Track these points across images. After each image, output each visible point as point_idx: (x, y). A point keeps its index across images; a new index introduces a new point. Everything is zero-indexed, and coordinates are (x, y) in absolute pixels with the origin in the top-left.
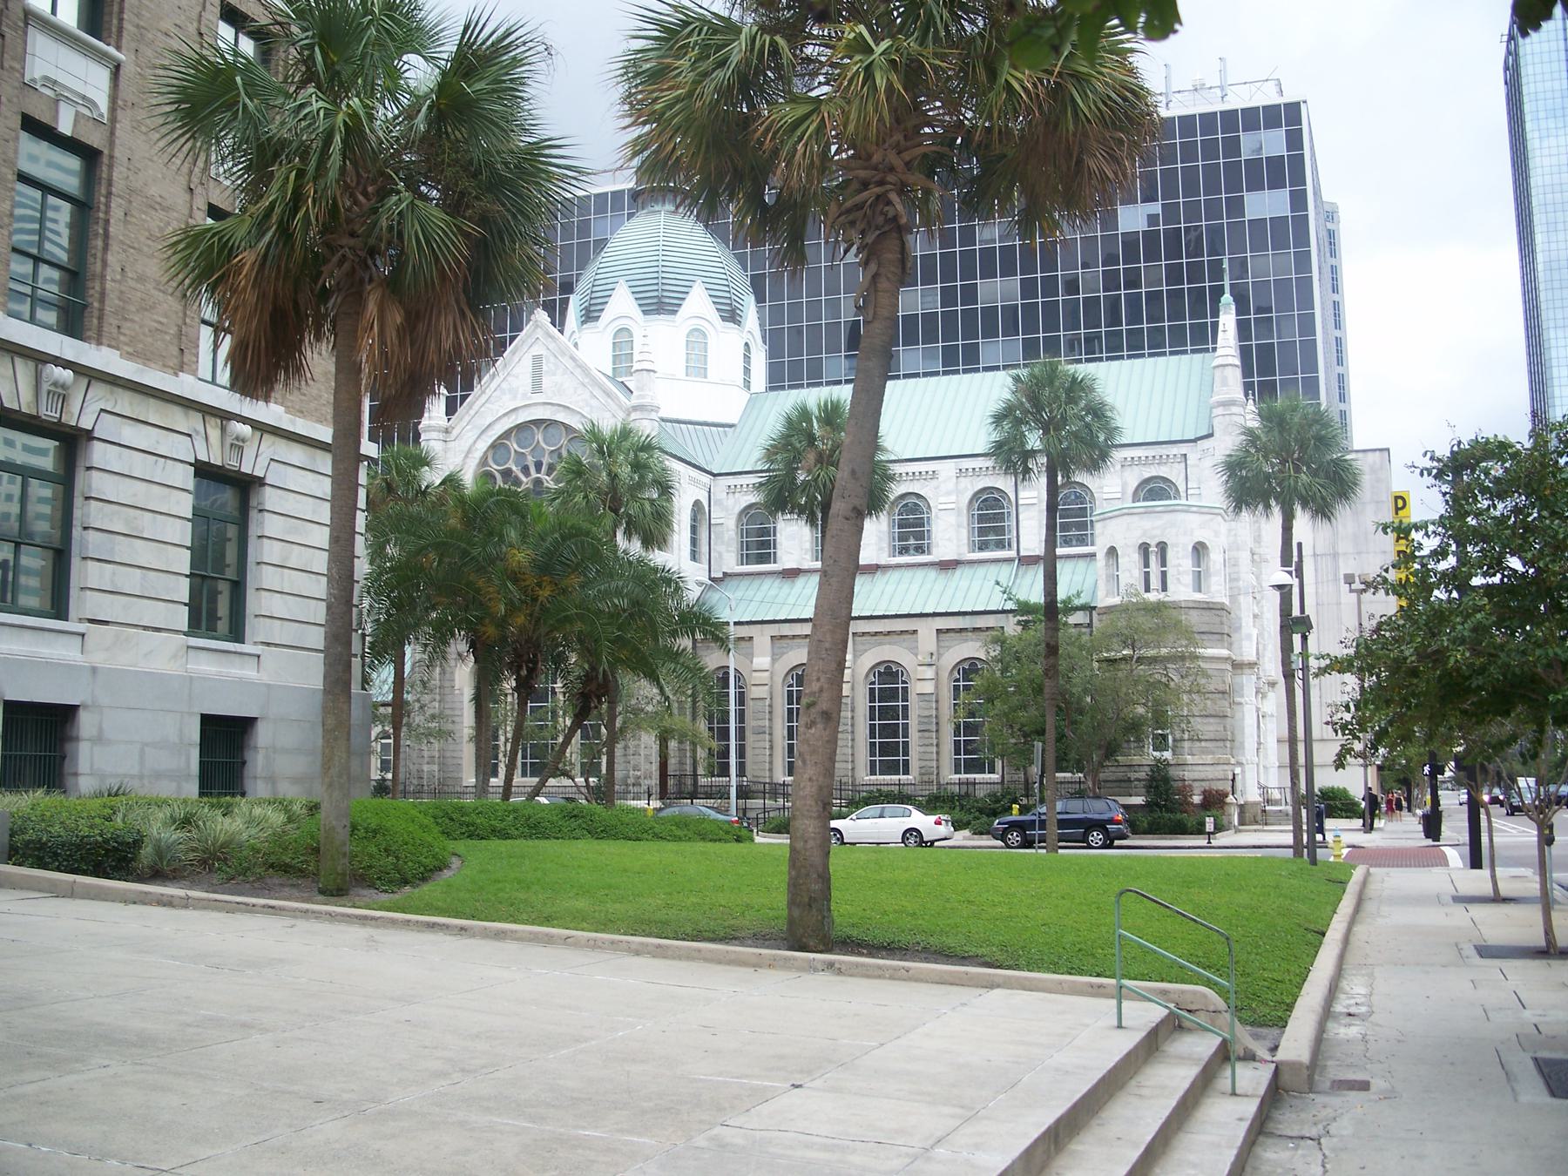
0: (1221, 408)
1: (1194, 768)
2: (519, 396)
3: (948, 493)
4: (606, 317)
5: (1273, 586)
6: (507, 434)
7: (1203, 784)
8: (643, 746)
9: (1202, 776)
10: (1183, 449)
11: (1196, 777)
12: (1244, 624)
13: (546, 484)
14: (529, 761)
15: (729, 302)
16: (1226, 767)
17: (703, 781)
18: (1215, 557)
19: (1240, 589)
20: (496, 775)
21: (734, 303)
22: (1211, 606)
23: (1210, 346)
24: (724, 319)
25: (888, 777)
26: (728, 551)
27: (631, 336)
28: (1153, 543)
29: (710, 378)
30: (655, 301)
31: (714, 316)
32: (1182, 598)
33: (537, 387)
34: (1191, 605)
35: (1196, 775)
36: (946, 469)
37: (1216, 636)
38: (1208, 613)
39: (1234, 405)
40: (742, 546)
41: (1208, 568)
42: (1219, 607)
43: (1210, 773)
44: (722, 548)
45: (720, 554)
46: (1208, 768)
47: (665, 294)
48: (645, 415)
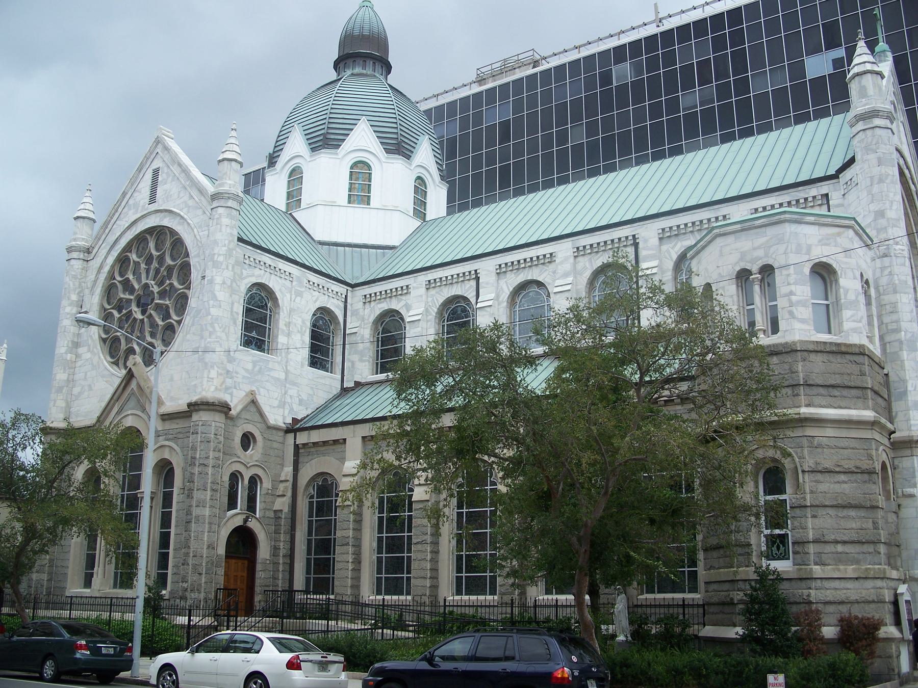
0: (861, 123)
1: (827, 584)
2: (140, 208)
3: (566, 275)
5: (854, 156)
6: (128, 248)
7: (840, 607)
8: (191, 555)
9: (840, 595)
10: (824, 188)
11: (830, 598)
12: (910, 388)
13: (151, 289)
14: (464, 575)
15: (395, 136)
16: (879, 583)
17: (299, 597)
18: (849, 284)
19: (901, 342)
20: (166, 589)
21: (400, 137)
22: (843, 349)
24: (388, 151)
25: (473, 598)
26: (361, 360)
28: (755, 268)
30: (321, 138)
31: (377, 147)
32: (797, 337)
33: (153, 199)
34: (811, 347)
35: (829, 595)
36: (564, 249)
37: (854, 392)
38: (839, 359)
39: (877, 116)
40: (377, 356)
41: (838, 300)
42: (857, 351)
43: (853, 591)
44: (355, 358)
45: (353, 363)
46: (849, 585)
48: (222, 203)
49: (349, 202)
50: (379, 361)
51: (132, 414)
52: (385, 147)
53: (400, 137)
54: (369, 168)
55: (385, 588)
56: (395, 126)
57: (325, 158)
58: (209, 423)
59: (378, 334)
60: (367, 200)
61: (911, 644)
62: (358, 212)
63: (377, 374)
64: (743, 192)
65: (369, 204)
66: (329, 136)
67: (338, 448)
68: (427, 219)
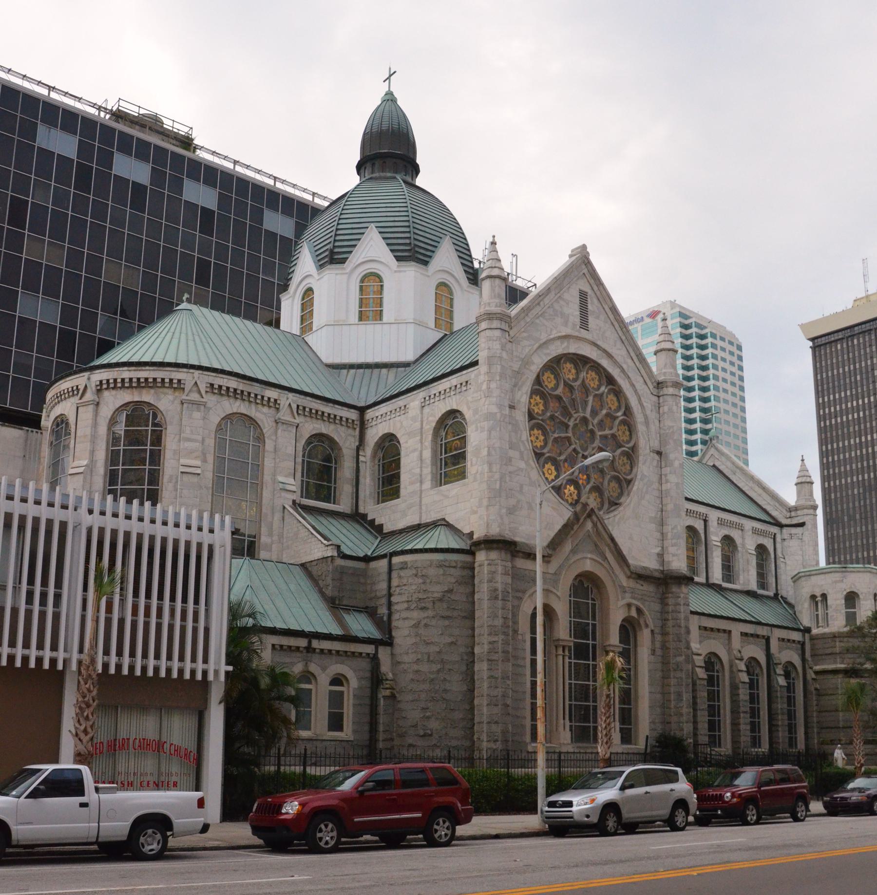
15: (408, 241)
29: (385, 318)
30: (327, 253)
31: (388, 257)
36: (414, 401)
50: (333, 485)
51: (590, 559)
54: (381, 281)
56: (408, 230)
57: (332, 274)
59: (379, 461)
60: (379, 315)
62: (370, 329)
63: (378, 504)
65: (381, 319)
67: (378, 317)
68: (456, 328)
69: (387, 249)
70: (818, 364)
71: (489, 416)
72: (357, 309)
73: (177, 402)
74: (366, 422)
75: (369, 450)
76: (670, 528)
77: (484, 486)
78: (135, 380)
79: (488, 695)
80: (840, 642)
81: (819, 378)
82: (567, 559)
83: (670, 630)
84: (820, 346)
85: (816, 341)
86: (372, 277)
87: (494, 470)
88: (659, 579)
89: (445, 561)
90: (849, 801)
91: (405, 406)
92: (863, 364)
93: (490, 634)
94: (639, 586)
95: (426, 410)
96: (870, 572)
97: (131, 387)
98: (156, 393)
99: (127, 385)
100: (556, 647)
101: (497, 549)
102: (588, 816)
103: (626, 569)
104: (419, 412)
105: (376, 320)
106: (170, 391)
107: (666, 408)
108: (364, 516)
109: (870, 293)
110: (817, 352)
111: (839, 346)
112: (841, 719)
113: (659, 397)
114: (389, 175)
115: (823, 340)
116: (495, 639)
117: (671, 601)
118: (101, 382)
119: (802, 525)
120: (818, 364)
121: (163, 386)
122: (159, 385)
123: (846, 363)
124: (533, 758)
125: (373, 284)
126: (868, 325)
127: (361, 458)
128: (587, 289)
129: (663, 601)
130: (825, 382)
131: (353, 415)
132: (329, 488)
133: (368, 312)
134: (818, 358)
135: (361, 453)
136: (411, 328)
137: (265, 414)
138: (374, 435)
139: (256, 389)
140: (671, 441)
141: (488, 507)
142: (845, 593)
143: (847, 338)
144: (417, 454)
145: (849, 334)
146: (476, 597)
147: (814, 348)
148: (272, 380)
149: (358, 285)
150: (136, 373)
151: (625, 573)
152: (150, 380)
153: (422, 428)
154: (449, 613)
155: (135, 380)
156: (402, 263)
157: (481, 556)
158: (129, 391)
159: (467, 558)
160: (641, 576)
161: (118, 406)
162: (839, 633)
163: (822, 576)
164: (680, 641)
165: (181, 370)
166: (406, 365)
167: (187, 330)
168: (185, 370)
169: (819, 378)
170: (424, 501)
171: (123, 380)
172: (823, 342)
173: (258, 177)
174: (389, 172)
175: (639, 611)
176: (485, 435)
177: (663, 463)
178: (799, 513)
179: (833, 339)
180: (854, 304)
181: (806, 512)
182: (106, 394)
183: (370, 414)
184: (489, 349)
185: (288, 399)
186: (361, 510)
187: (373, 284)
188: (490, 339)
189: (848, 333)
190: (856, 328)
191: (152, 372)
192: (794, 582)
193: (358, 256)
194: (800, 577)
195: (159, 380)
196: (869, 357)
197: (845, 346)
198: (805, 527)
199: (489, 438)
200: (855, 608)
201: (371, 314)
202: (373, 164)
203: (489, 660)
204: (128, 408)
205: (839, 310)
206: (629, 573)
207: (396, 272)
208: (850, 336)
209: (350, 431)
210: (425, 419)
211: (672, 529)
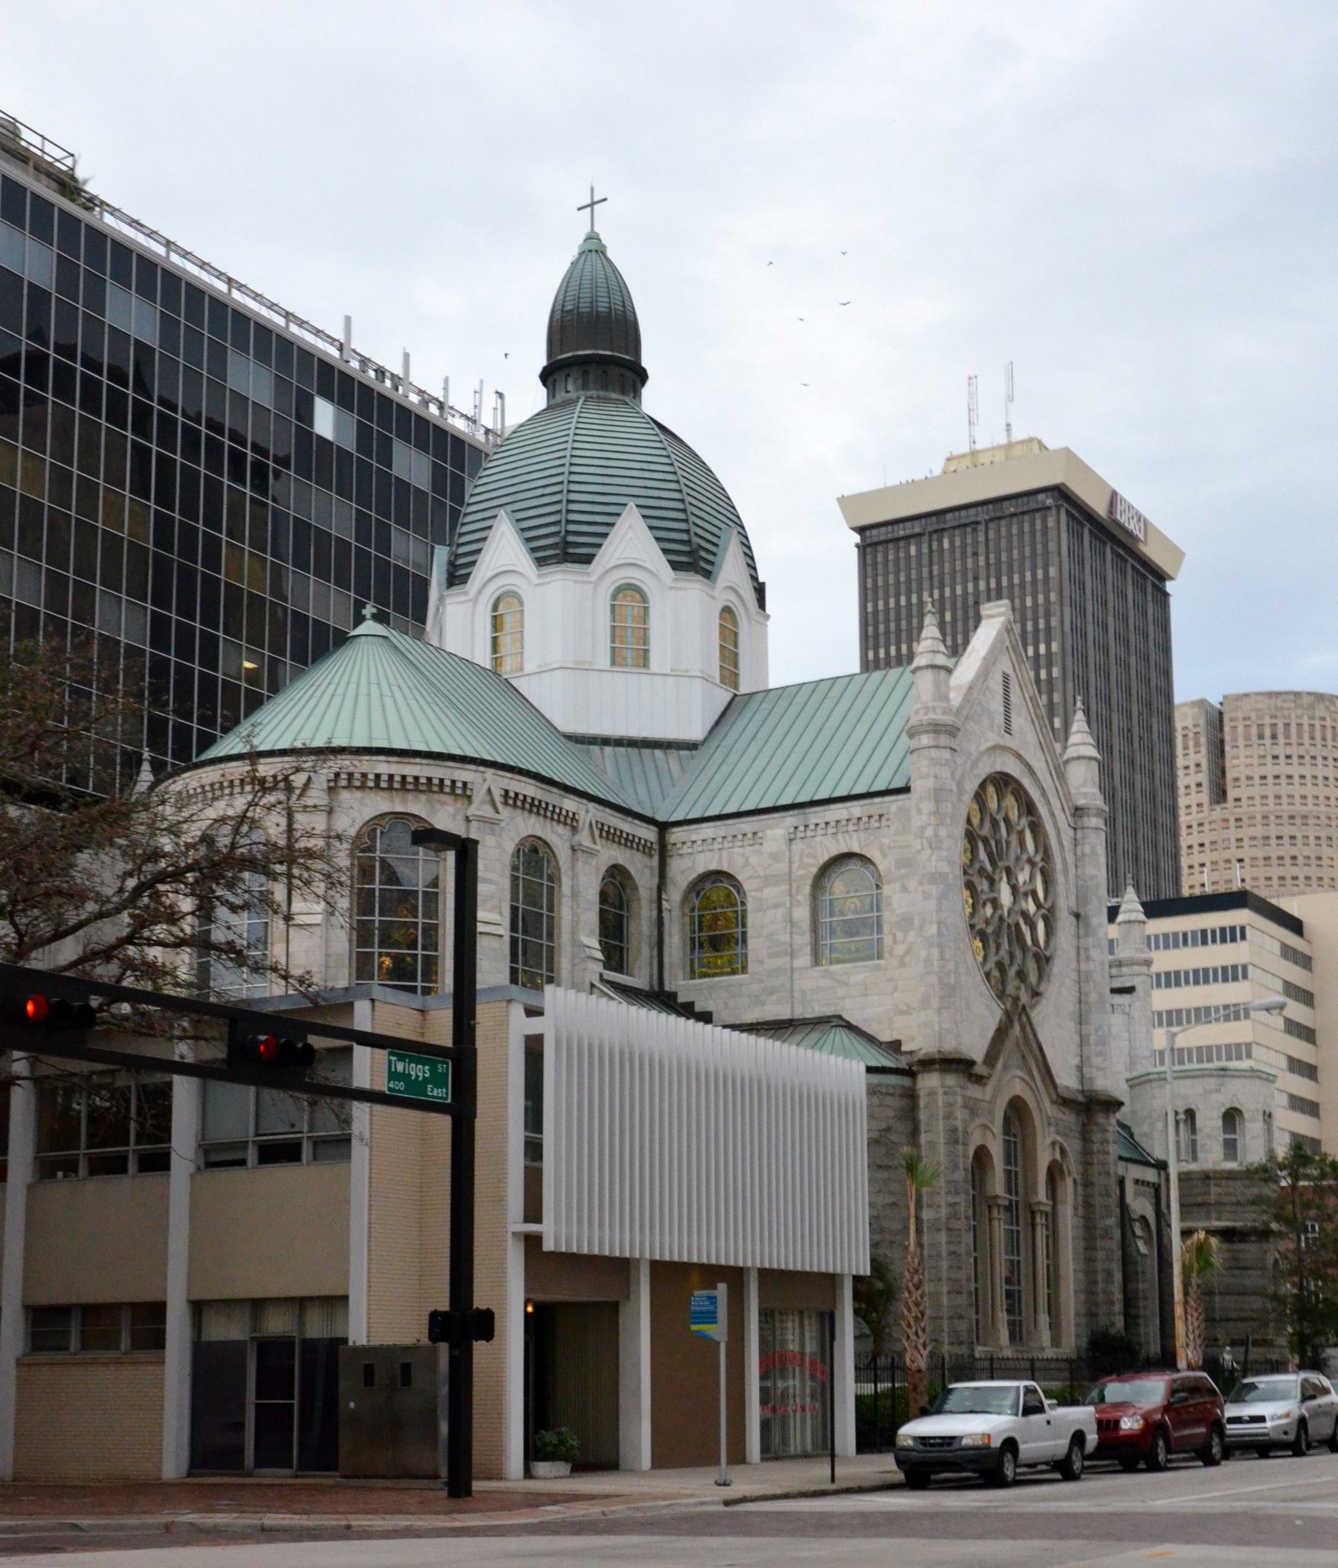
4: (480, 574)
15: (685, 537)
21: (695, 540)
23: (419, 984)
24: (675, 566)
27: (521, 603)
29: (654, 665)
30: (556, 540)
31: (659, 563)
36: (777, 829)
47: (572, 527)
49: (613, 663)
52: (535, 544)
53: (695, 540)
54: (644, 598)
55: (253, 425)
58: (1285, 712)
60: (643, 659)
61: (41, 1057)
64: (762, 805)
65: (645, 663)
66: (571, 539)
67: (641, 661)
69: (655, 548)
70: (869, 581)
71: (935, 878)
72: (608, 644)
73: (460, 817)
74: (669, 847)
75: (674, 895)
76: (1092, 1028)
77: (934, 979)
78: (397, 778)
79: (949, 1279)
80: (1217, 1185)
81: (870, 608)
82: (1000, 1080)
83: (1096, 1179)
84: (875, 544)
85: (868, 533)
86: (629, 592)
87: (947, 956)
88: (1080, 1104)
89: (880, 1085)
90: (955, 1446)
91: (755, 834)
92: (959, 590)
93: (948, 1193)
94: (1060, 1115)
95: (798, 846)
96: (1260, 1078)
97: (390, 788)
98: (428, 801)
99: (384, 785)
100: (990, 1207)
101: (956, 1071)
102: (1286, 1433)
103: (1052, 1091)
104: (784, 847)
105: (638, 666)
106: (449, 799)
107: (1087, 849)
108: (673, 996)
109: (979, 446)
110: (868, 557)
111: (913, 550)
112: (1217, 1306)
113: (1075, 829)
114: (614, 396)
115: (882, 534)
116: (957, 1199)
117: (1097, 1136)
118: (337, 775)
119: (1130, 990)
120: (869, 581)
121: (441, 791)
122: (411, 787)
123: (926, 584)
124: (987, 1364)
125: (630, 606)
126: (972, 511)
127: (665, 905)
128: (1010, 672)
129: (1085, 1137)
130: (881, 618)
131: (649, 834)
132: (621, 949)
133: (624, 652)
134: (869, 569)
135: (664, 896)
136: (698, 685)
137: (560, 836)
138: (685, 868)
139: (553, 797)
140: (1094, 898)
141: (939, 1010)
142: (1223, 1110)
143: (930, 534)
144: (780, 912)
145: (935, 527)
146: (923, 1139)
147: (863, 548)
148: (471, 753)
149: (608, 603)
150: (400, 766)
151: (1050, 1095)
152: (423, 780)
153: (790, 872)
154: (887, 1162)
155: (397, 778)
156: (682, 575)
157: (929, 1082)
158: (386, 794)
159: (905, 1081)
160: (1064, 1102)
161: (367, 818)
162: (1215, 1172)
163: (1188, 1082)
164: (1109, 1196)
165: (468, 766)
166: (692, 746)
167: (378, 677)
168: (473, 767)
169: (870, 608)
170: (797, 984)
171: (378, 776)
172: (882, 538)
173: (264, 312)
174: (614, 391)
175: (1063, 1151)
176: (932, 904)
177: (1082, 932)
178: (1124, 970)
179: (902, 533)
180: (946, 466)
181: (1137, 969)
182: (345, 796)
183: (676, 835)
184: (936, 777)
185: (485, 780)
186: (667, 988)
187: (630, 606)
188: (935, 762)
189: (932, 524)
190: (949, 516)
191: (425, 768)
192: (1131, 1087)
193: (611, 553)
194: (1150, 1081)
195: (436, 781)
196: (970, 577)
197: (925, 550)
198: (1135, 994)
199: (939, 910)
200: (1234, 1132)
201: (629, 655)
202: (586, 372)
203: (948, 1229)
204: (383, 823)
205: (919, 476)
206: (1055, 1097)
207: (671, 588)
208: (935, 531)
209: (646, 859)
210: (796, 858)
211: (1097, 1030)
